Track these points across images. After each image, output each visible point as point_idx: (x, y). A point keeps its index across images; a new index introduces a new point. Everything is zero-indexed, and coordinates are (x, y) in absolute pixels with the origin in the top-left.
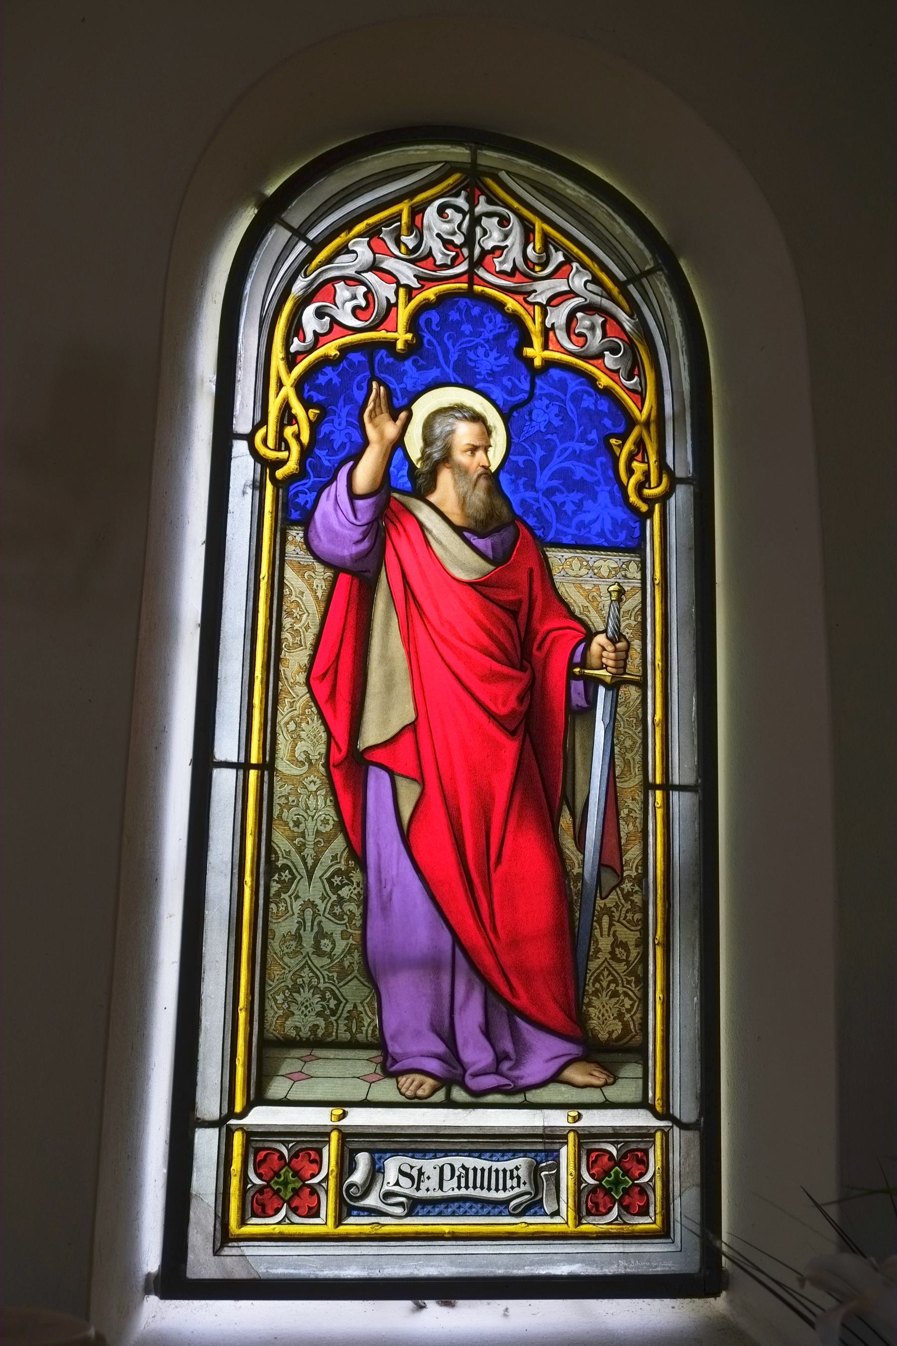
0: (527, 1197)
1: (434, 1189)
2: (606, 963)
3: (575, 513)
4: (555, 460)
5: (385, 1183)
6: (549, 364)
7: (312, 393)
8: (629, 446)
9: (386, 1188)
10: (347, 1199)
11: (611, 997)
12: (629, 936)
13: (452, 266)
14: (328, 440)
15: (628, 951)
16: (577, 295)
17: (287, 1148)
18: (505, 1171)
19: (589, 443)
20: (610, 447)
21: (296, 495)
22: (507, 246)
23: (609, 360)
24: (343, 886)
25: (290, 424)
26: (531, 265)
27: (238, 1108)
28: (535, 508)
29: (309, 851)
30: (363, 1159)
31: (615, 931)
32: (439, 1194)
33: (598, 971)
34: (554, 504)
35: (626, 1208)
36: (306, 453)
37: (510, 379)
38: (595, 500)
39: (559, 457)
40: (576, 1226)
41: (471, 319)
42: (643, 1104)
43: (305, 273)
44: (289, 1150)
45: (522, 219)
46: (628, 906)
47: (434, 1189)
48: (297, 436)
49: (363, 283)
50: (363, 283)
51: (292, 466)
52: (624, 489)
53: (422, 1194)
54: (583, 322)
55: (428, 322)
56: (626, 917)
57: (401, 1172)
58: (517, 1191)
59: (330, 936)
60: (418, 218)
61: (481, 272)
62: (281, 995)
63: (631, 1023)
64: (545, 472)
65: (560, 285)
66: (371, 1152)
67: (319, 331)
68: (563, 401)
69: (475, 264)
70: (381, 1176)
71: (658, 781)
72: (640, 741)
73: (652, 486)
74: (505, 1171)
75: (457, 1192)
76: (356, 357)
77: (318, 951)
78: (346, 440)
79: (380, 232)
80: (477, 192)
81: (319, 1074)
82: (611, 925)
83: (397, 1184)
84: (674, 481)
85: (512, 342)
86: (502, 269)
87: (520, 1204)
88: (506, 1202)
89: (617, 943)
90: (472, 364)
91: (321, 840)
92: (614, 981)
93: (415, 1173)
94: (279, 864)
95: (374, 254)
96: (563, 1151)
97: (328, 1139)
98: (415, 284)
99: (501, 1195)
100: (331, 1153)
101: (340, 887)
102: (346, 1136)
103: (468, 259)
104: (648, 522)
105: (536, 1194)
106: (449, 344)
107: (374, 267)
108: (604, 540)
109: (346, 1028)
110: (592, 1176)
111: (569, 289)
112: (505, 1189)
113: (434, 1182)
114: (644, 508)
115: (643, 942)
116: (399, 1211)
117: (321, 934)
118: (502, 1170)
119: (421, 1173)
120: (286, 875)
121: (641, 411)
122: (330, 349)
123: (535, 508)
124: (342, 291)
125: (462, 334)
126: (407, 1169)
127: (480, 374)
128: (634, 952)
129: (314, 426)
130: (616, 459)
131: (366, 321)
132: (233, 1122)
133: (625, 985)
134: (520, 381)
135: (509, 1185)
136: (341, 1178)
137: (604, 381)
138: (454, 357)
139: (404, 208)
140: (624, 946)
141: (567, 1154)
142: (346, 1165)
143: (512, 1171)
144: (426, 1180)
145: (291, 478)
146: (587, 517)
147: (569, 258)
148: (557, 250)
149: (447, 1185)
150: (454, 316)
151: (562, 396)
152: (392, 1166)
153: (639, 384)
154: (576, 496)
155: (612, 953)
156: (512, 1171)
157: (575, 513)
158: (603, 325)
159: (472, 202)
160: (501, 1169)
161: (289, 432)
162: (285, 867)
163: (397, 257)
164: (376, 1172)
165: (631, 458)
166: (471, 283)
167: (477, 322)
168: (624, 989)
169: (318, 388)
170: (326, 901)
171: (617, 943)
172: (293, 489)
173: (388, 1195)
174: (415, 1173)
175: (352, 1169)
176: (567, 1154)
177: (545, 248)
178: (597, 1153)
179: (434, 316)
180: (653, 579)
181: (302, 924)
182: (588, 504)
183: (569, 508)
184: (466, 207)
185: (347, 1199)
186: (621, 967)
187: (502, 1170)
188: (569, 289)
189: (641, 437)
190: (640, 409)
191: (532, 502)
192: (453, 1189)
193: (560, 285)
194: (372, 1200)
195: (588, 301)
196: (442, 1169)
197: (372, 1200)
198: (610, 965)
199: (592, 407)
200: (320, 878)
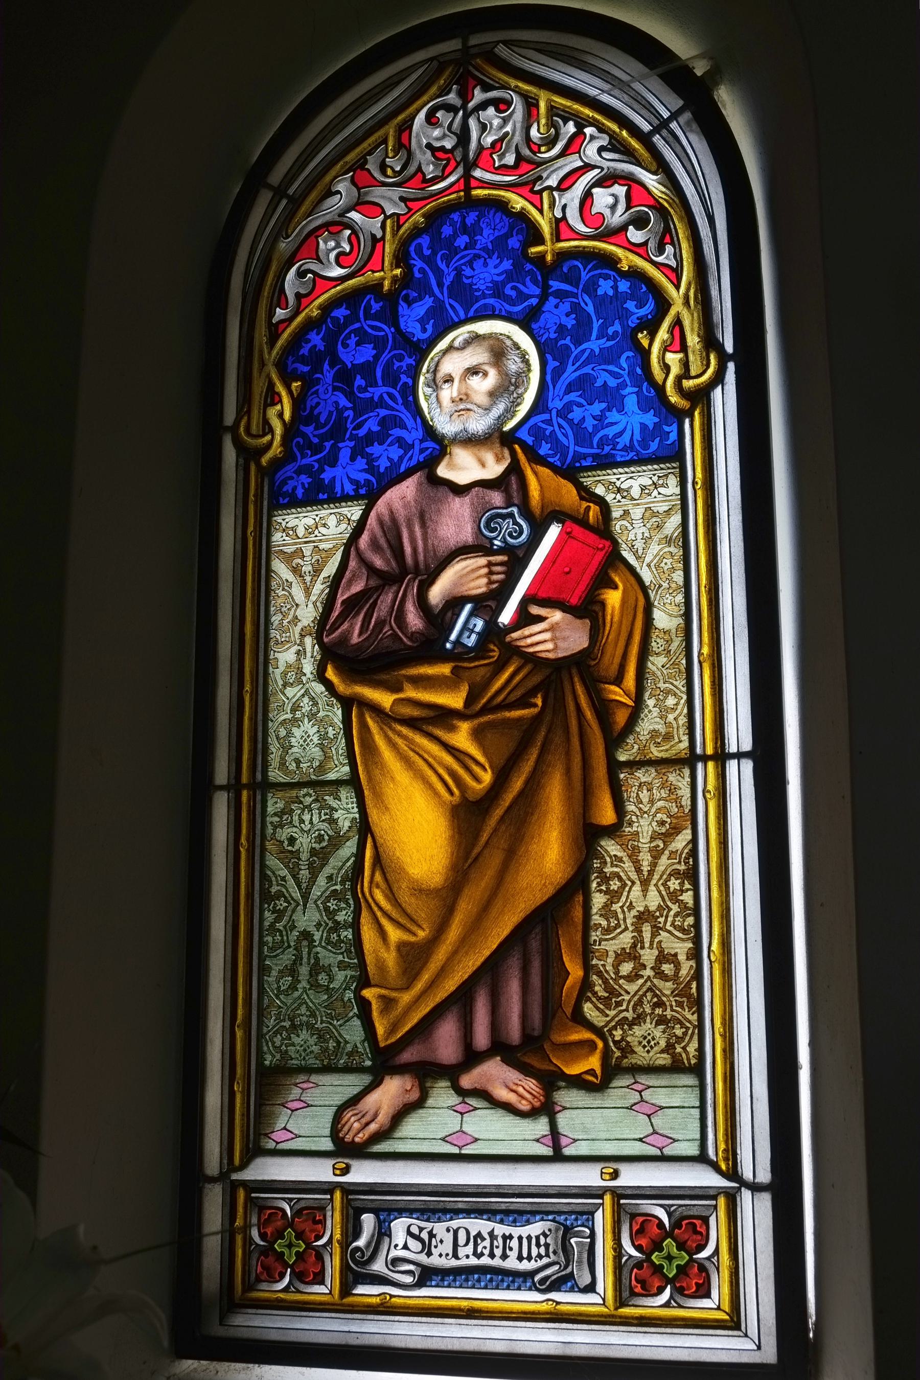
0: (556, 1267)
1: (447, 1255)
2: (649, 983)
3: (596, 429)
4: (570, 368)
5: (392, 1247)
6: (562, 256)
7: (295, 365)
8: (663, 334)
9: (394, 1253)
10: (352, 1265)
11: (657, 1024)
12: (681, 948)
13: (443, 178)
14: (312, 419)
15: (677, 966)
16: (594, 167)
17: (290, 1206)
18: (529, 1238)
19: (612, 338)
20: (637, 345)
21: (284, 482)
22: (507, 134)
23: (635, 236)
24: (340, 910)
25: (273, 404)
26: (535, 148)
27: (237, 1161)
28: (548, 433)
29: (304, 873)
30: (368, 1221)
31: (660, 942)
32: (454, 1263)
33: (640, 993)
34: (570, 422)
35: (679, 1291)
36: (290, 431)
37: (513, 288)
38: (621, 410)
39: (573, 365)
40: (616, 1309)
41: (465, 230)
42: (702, 1158)
43: (286, 234)
44: (291, 1208)
45: (525, 96)
46: (675, 908)
47: (447, 1255)
48: (281, 415)
49: (347, 226)
50: (347, 226)
51: (276, 449)
52: (660, 390)
53: (435, 1261)
54: (602, 198)
55: (419, 249)
56: (674, 921)
57: (409, 1233)
58: (545, 1261)
59: (328, 970)
60: (405, 136)
61: (478, 173)
62: (279, 1036)
63: (684, 1055)
64: (558, 385)
65: (574, 162)
66: (375, 1211)
67: (303, 292)
68: (575, 296)
69: (469, 167)
70: (387, 1240)
71: (710, 751)
72: (685, 697)
73: (693, 373)
74: (529, 1238)
75: (473, 1261)
76: (341, 313)
77: (314, 985)
78: (333, 409)
79: (366, 162)
80: (472, 82)
81: (316, 1103)
82: (654, 935)
83: (406, 1247)
84: (723, 359)
85: (514, 243)
86: (502, 163)
87: (547, 1278)
88: (532, 1274)
89: (663, 957)
90: (469, 281)
91: (315, 859)
92: (660, 1004)
93: (425, 1235)
94: (274, 889)
95: (359, 189)
96: (598, 1215)
97: (329, 1197)
98: (401, 209)
99: (526, 1266)
100: (334, 1226)
101: (335, 912)
102: (348, 1190)
103: (462, 163)
104: (687, 421)
105: (566, 1267)
106: (443, 266)
107: (359, 204)
108: (635, 453)
109: (295, 566)
110: (638, 1248)
111: (660, 383)
112: (529, 1258)
113: (448, 1247)
114: (683, 404)
115: (696, 954)
116: (408, 1279)
117: (316, 968)
118: (527, 1238)
119: (431, 1235)
120: (282, 904)
121: (678, 287)
122: (313, 310)
123: (548, 433)
124: (326, 245)
125: (456, 251)
126: (415, 1230)
127: (478, 290)
128: (686, 968)
129: (297, 404)
130: (645, 354)
131: (350, 267)
132: (235, 1176)
133: (674, 1008)
134: (526, 286)
135: (534, 1252)
136: (345, 1244)
137: (628, 259)
138: (447, 281)
139: (390, 130)
140: (673, 959)
141: (602, 1220)
142: (353, 1229)
143: (538, 1238)
144: (439, 1244)
145: (277, 464)
146: (611, 432)
147: (580, 127)
148: (565, 122)
149: (462, 1252)
150: (447, 231)
151: (575, 290)
152: (399, 1226)
153: (672, 257)
154: (597, 408)
155: (657, 969)
156: (538, 1238)
157: (596, 429)
158: (628, 196)
159: (465, 96)
160: (524, 1235)
161: (272, 412)
162: (280, 895)
163: (384, 184)
164: (383, 1232)
165: (666, 349)
166: (468, 189)
167: (472, 231)
168: (674, 1013)
169: (303, 360)
170: (321, 929)
171: (663, 957)
172: (280, 476)
173: (396, 1261)
174: (425, 1235)
175: (357, 1235)
176: (602, 1220)
177: (551, 124)
178: (645, 1218)
179: (425, 241)
180: (694, 483)
181: (298, 958)
182: (613, 416)
183: (589, 424)
184: (458, 102)
185: (352, 1265)
186: (667, 987)
187: (527, 1238)
188: (660, 383)
189: (678, 317)
190: (676, 282)
191: (544, 426)
192: (468, 1257)
193: (574, 162)
194: (379, 1266)
195: (605, 171)
196: (456, 1232)
197: (379, 1266)
198: (655, 986)
199: (611, 292)
200: (316, 901)
